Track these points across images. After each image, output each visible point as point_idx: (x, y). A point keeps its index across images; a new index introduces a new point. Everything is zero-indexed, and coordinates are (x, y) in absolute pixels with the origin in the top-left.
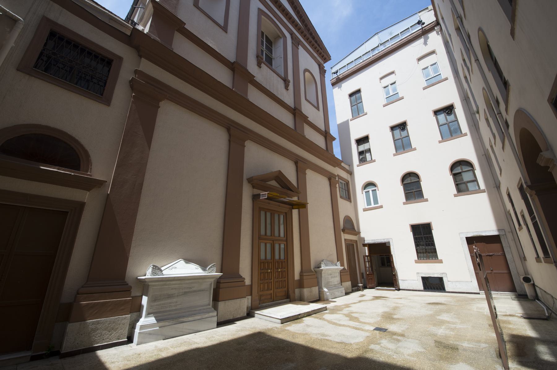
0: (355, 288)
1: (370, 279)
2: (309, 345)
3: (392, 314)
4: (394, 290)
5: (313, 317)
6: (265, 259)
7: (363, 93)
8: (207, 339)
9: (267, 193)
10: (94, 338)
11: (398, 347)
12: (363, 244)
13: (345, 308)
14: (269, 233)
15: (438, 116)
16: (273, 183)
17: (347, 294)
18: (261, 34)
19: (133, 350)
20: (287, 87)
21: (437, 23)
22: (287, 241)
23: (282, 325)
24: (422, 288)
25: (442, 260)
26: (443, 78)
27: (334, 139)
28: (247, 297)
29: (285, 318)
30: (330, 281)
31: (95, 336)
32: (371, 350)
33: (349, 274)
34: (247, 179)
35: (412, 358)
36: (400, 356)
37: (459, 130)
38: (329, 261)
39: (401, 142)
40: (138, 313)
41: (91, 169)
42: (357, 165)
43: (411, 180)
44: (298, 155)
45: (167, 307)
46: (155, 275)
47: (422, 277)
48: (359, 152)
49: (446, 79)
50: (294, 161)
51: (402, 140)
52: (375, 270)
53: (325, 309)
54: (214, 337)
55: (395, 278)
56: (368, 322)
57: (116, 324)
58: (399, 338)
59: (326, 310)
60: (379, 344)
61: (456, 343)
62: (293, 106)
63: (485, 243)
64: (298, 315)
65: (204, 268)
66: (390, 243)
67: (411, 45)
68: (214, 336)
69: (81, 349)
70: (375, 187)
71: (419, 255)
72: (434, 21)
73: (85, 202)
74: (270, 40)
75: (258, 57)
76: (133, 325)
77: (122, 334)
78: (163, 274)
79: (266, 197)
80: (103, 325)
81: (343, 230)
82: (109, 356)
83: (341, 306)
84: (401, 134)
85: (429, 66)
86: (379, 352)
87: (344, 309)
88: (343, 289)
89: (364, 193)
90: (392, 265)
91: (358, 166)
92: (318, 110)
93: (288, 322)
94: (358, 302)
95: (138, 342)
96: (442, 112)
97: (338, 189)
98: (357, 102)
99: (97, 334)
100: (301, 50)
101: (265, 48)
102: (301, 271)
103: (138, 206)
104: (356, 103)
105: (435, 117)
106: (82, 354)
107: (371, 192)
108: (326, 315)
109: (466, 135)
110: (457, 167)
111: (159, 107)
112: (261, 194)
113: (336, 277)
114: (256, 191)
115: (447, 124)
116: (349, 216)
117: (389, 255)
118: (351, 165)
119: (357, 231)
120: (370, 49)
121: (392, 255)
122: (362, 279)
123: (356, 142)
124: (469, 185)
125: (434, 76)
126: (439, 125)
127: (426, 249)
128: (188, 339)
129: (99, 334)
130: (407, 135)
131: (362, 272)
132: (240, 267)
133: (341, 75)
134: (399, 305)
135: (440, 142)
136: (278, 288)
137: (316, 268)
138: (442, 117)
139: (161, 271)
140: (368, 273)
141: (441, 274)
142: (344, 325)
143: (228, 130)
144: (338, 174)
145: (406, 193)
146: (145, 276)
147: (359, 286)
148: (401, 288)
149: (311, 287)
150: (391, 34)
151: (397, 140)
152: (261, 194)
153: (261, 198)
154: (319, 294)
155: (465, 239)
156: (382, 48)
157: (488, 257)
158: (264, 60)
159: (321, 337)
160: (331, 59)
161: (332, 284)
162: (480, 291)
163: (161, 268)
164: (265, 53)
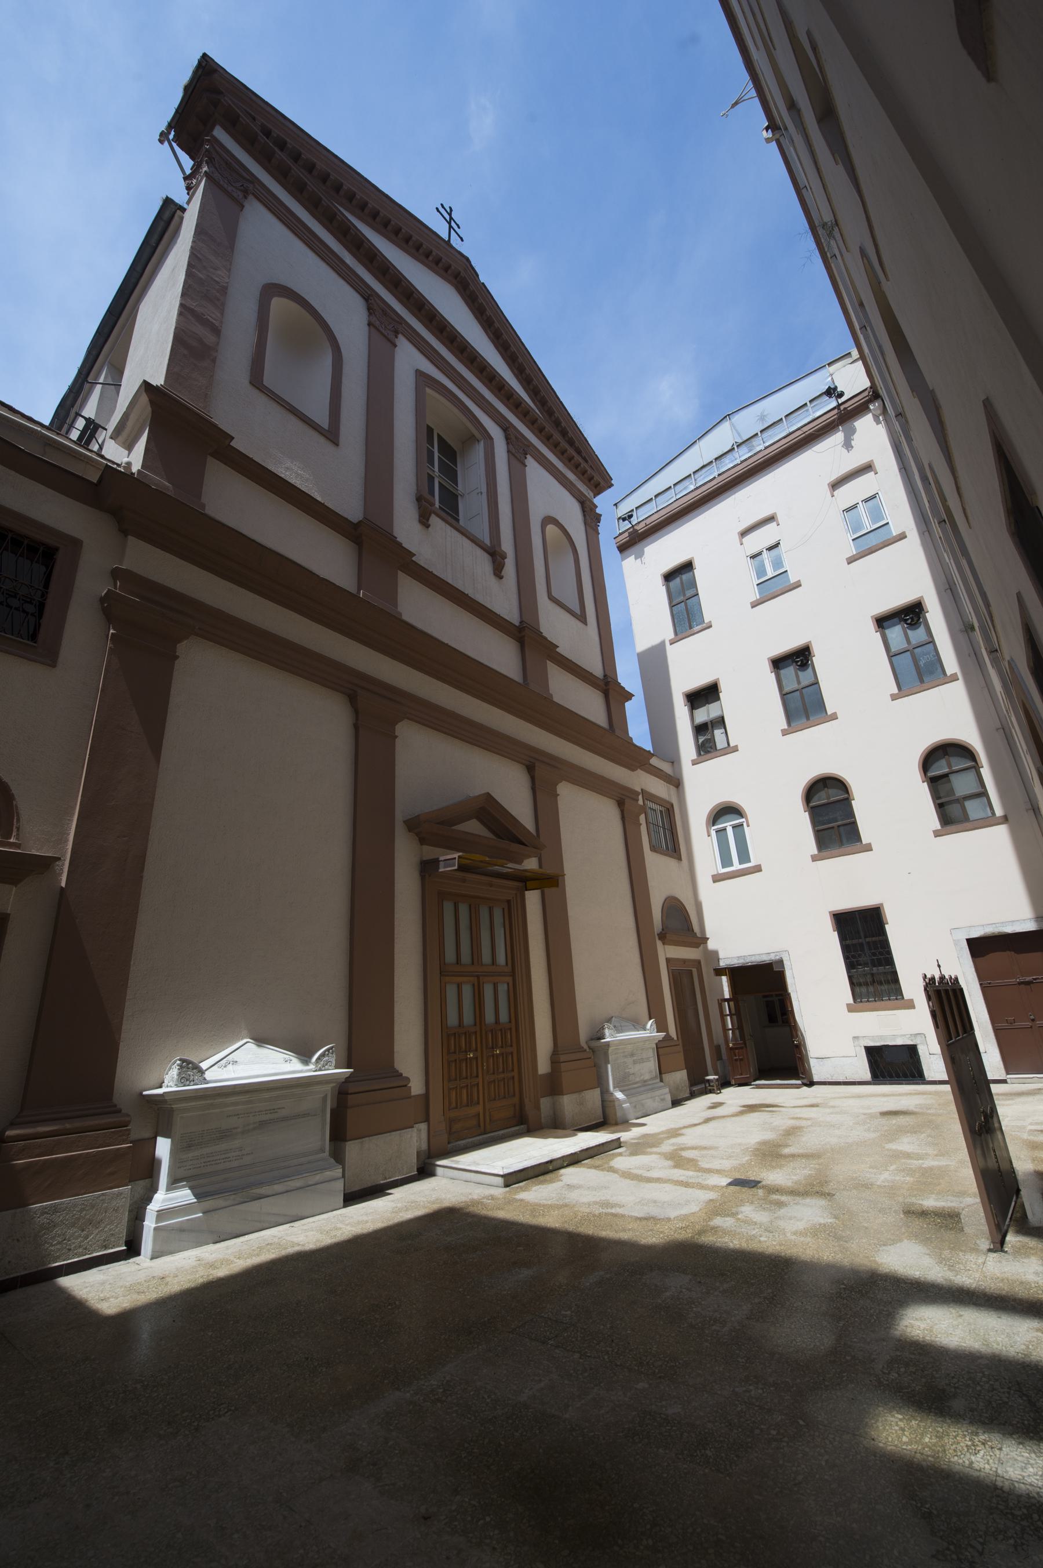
0: (698, 1086)
1: (736, 1060)
2: (571, 1228)
3: (780, 1146)
4: (797, 1087)
5: (584, 1166)
6: (460, 1026)
7: (700, 574)
8: (321, 1233)
9: (456, 855)
10: (47, 1249)
11: (776, 1218)
12: (714, 969)
13: (668, 1138)
14: (466, 958)
15: (887, 631)
16: (473, 827)
17: (676, 1103)
18: (427, 434)
19: (146, 1270)
20: (498, 571)
21: (874, 394)
22: (513, 974)
23: (508, 1189)
24: (867, 1076)
25: (912, 1001)
26: (894, 534)
27: (629, 696)
28: (417, 1125)
29: (515, 1172)
30: (632, 1071)
31: (48, 1243)
32: (713, 1228)
33: (682, 1050)
34: (405, 822)
35: (802, 1239)
36: (777, 1236)
37: (938, 666)
38: (627, 1020)
39: (799, 698)
40: (147, 1180)
41: (18, 829)
42: (692, 761)
43: (828, 798)
44: (534, 748)
45: (219, 1161)
46: (188, 1082)
47: (865, 1047)
48: (696, 727)
49: (902, 537)
50: (524, 764)
51: (802, 694)
52: (750, 1035)
53: (617, 1144)
54: (341, 1228)
55: (801, 1053)
56: (718, 1167)
57: (97, 1210)
58: (784, 1198)
59: (620, 1147)
60: (734, 1215)
61: (910, 1201)
62: (516, 621)
63: (1013, 953)
64: (547, 1162)
65: (306, 1059)
66: (785, 962)
67: (814, 449)
68: (339, 1225)
69: (18, 1277)
70: (739, 817)
71: (857, 989)
72: (866, 389)
73: (9, 912)
74: (450, 446)
75: (419, 499)
76: (137, 1212)
77: (112, 1234)
78: (205, 1079)
79: (456, 868)
80: (67, 1214)
81: (662, 937)
82: (89, 1288)
83: (659, 1134)
84: (797, 677)
85: (860, 503)
86: (731, 1231)
87: (665, 1142)
88: (667, 1090)
89: (713, 833)
90: (792, 1020)
91: (695, 763)
92: (585, 623)
93: (522, 1181)
94: (701, 1121)
95: (153, 1251)
96: (896, 620)
97: (643, 828)
98: (684, 595)
99: (53, 1238)
100: (533, 470)
101: (439, 471)
102: (554, 1051)
103: (137, 912)
104: (682, 598)
105: (878, 633)
106: (21, 1287)
107: (730, 832)
108: (619, 1159)
109: (954, 678)
110: (935, 762)
111: (177, 657)
112: (442, 858)
113: (648, 1059)
114: (430, 852)
115: (910, 650)
116: (677, 896)
117: (781, 995)
118: (675, 761)
119: (699, 935)
120: (712, 458)
121: (789, 994)
122: (718, 1063)
123: (686, 699)
124: (970, 805)
125: (872, 529)
126: (891, 654)
127: (872, 975)
128: (275, 1237)
129: (59, 1236)
130: (812, 680)
131: (715, 1043)
132: (395, 1050)
133: (642, 525)
134: (803, 1123)
135: (894, 697)
136: (495, 1099)
137: (592, 1039)
138: (896, 633)
139: (202, 1072)
140: (731, 1045)
141: (913, 1038)
142: (658, 1180)
143: (352, 699)
144: (643, 788)
145: (818, 831)
146: (161, 1087)
147: (708, 1081)
148: (816, 1079)
149: (583, 1091)
150: (762, 418)
151: (790, 693)
152: (442, 858)
153: (440, 870)
154: (604, 1107)
155: (965, 943)
156: (743, 454)
157: (1022, 986)
158: (437, 505)
159: (601, 1210)
160: (612, 485)
161: (638, 1079)
162: (1008, 1073)
163: (201, 1064)
164: (439, 482)
